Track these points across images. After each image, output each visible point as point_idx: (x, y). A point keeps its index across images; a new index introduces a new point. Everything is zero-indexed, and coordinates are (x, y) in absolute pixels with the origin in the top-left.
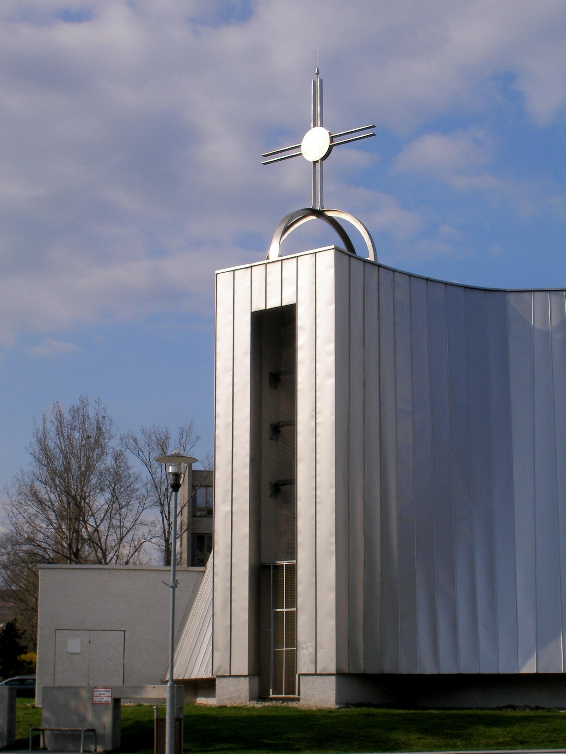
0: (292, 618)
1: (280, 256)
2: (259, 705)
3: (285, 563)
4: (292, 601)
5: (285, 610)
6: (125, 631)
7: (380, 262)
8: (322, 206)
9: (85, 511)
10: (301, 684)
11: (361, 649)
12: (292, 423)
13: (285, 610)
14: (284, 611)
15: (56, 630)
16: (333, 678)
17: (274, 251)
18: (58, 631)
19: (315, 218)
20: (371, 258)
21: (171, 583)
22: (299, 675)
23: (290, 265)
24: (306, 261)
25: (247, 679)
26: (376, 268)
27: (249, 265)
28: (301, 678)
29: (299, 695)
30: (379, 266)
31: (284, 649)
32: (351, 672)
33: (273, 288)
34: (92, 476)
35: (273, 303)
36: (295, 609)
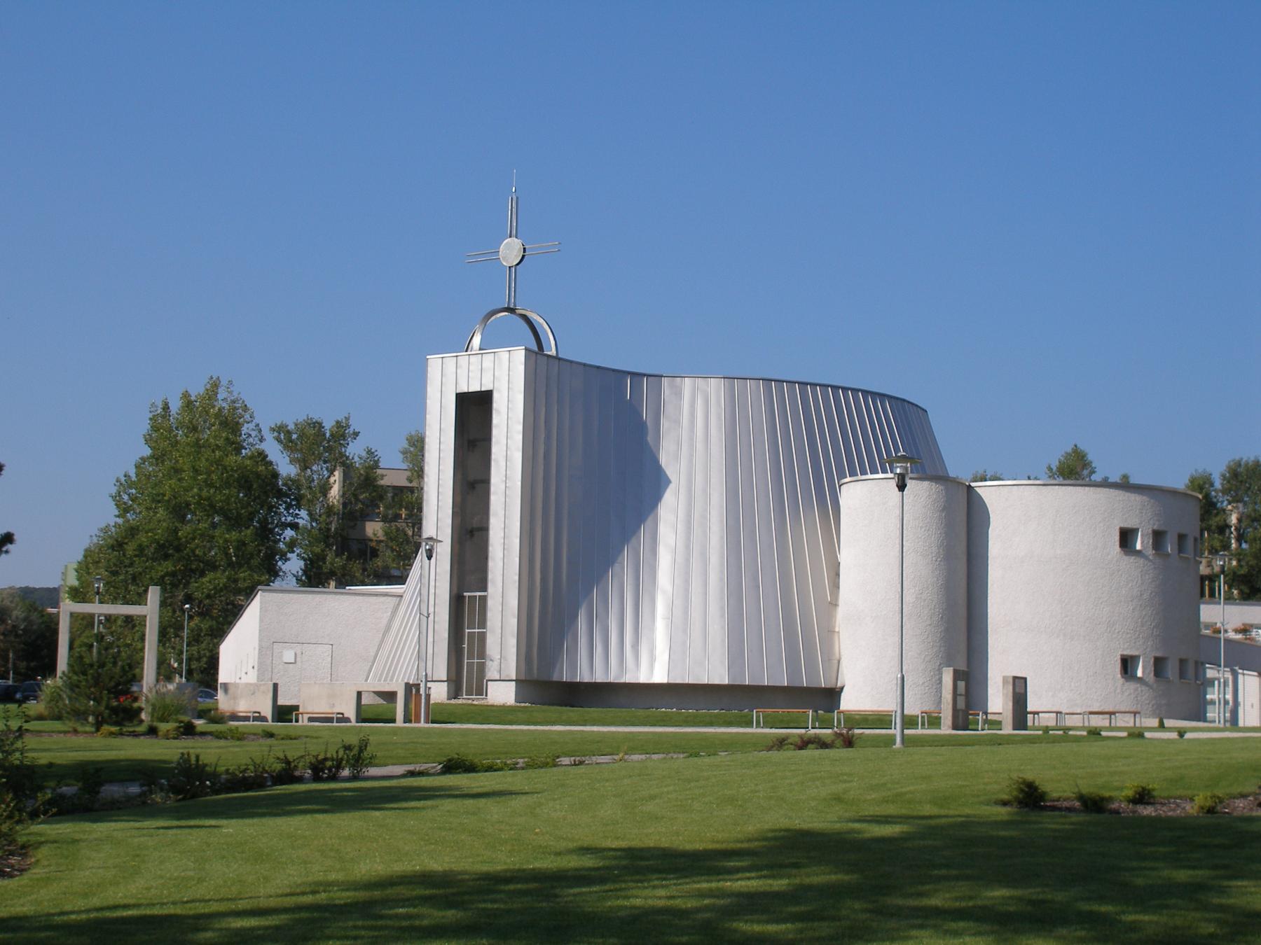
0: (482, 638)
1: (480, 349)
2: (518, 704)
3: (478, 594)
4: (483, 623)
5: (477, 630)
6: (332, 645)
7: (560, 356)
8: (515, 305)
9: (1083, 728)
10: (489, 687)
11: (535, 667)
12: (486, 481)
13: (477, 630)
14: (861, 475)
15: (295, 663)
16: (514, 683)
17: (477, 341)
18: (293, 661)
19: (506, 313)
20: (553, 352)
21: (426, 615)
22: (487, 681)
23: (488, 359)
24: (503, 353)
25: (446, 683)
26: (558, 360)
27: (455, 354)
28: (489, 683)
29: (486, 696)
30: (560, 359)
31: (476, 661)
32: (527, 679)
33: (475, 374)
34: (1064, 806)
35: (475, 388)
36: (485, 630)
